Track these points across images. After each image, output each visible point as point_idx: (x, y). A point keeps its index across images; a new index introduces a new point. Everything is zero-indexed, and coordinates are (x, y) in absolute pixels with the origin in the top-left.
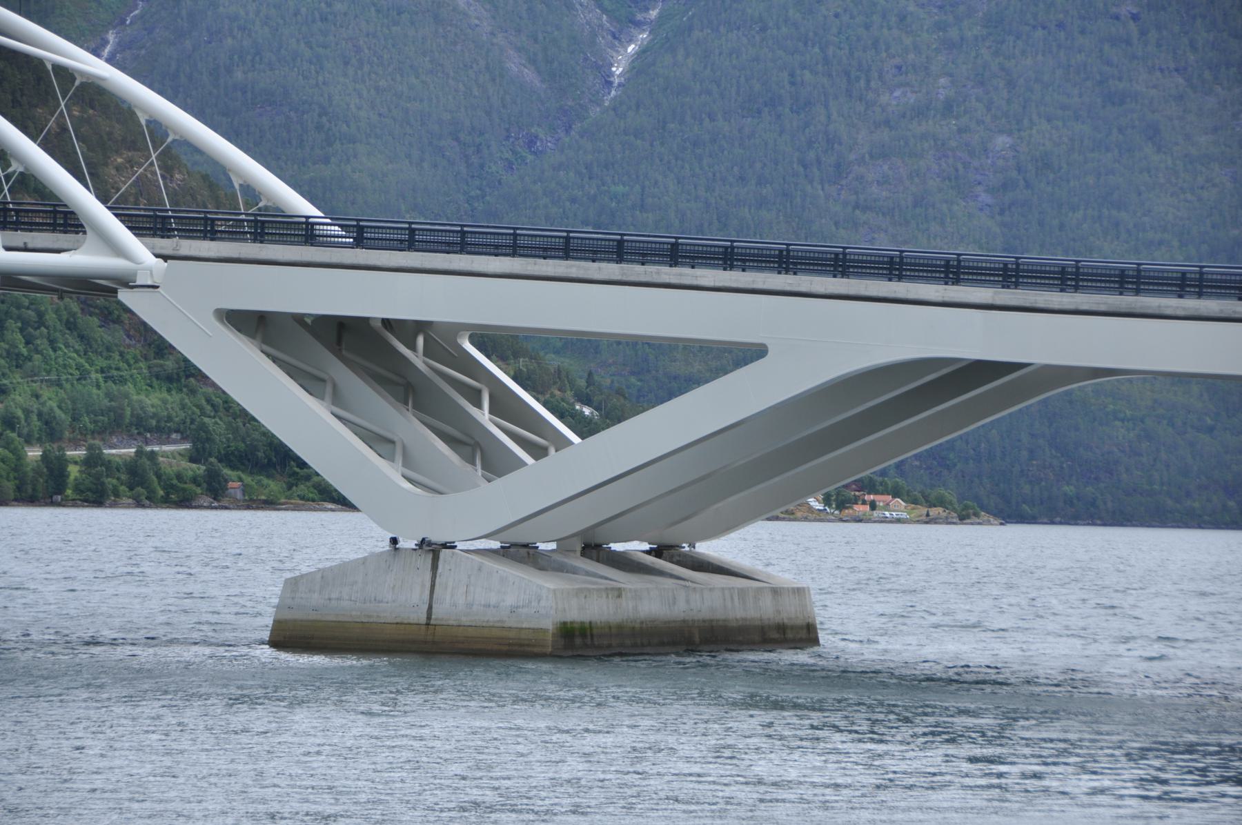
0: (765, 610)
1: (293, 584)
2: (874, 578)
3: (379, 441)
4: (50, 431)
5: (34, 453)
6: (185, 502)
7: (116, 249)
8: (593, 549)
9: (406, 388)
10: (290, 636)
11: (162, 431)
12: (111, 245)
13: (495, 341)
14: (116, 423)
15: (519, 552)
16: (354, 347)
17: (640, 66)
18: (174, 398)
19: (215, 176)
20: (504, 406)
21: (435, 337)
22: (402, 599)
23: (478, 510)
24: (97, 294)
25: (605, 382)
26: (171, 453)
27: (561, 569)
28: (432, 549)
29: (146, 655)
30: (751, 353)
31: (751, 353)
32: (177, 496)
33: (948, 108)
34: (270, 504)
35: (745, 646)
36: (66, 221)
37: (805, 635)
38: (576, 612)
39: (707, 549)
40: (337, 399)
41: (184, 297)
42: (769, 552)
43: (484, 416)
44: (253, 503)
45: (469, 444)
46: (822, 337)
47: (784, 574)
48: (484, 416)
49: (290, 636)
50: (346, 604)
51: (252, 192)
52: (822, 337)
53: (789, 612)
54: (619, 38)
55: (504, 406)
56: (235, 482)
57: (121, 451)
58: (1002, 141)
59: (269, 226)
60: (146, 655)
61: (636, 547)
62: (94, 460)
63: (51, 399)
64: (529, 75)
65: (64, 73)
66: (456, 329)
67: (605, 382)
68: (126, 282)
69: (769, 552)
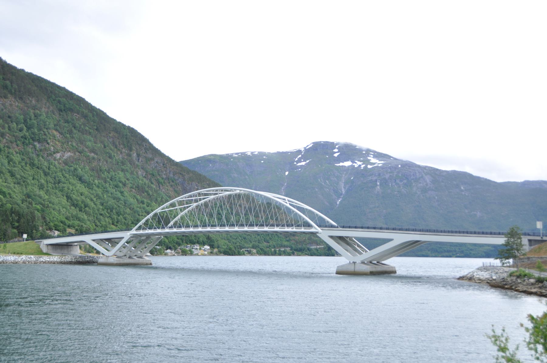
0: (391, 269)
1: (338, 267)
2: (401, 264)
3: (347, 250)
4: (274, 247)
5: (273, 250)
6: (290, 255)
7: (316, 229)
8: (371, 262)
9: (348, 244)
10: (338, 273)
11: (287, 247)
12: (316, 228)
13: (357, 238)
14: (282, 246)
15: (363, 263)
16: (341, 239)
17: (340, 202)
18: (288, 243)
19: (324, 220)
20: (359, 246)
21: (351, 238)
22: (351, 268)
23: (359, 258)
24: (314, 234)
25: (371, 244)
26: (288, 249)
27: (368, 265)
28: (354, 263)
29: (329, 275)
30: (391, 240)
31: (391, 240)
32: (289, 255)
33: (378, 207)
34: (300, 255)
35: (387, 273)
36: (309, 226)
37: (151, 264)
38: (371, 270)
39: (383, 262)
40: (341, 246)
41: (324, 234)
42: (393, 262)
43: (356, 247)
44: (298, 255)
45: (356, 250)
46: (400, 238)
47: (392, 265)
48: (356, 247)
49: (338, 273)
50: (344, 269)
51: (328, 222)
52: (400, 238)
53: (393, 270)
54: (338, 199)
55: (359, 246)
56: (296, 253)
57: (283, 249)
58: (384, 211)
59: (332, 226)
60: (329, 275)
61: (375, 262)
62: (279, 250)
63: (274, 243)
64: (328, 204)
65: (306, 209)
66: (352, 237)
67: (371, 244)
68: (317, 233)
69: (393, 262)
